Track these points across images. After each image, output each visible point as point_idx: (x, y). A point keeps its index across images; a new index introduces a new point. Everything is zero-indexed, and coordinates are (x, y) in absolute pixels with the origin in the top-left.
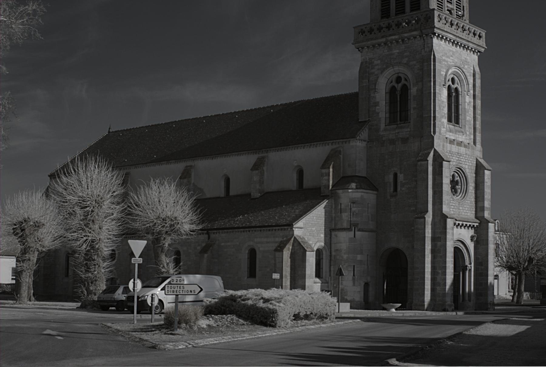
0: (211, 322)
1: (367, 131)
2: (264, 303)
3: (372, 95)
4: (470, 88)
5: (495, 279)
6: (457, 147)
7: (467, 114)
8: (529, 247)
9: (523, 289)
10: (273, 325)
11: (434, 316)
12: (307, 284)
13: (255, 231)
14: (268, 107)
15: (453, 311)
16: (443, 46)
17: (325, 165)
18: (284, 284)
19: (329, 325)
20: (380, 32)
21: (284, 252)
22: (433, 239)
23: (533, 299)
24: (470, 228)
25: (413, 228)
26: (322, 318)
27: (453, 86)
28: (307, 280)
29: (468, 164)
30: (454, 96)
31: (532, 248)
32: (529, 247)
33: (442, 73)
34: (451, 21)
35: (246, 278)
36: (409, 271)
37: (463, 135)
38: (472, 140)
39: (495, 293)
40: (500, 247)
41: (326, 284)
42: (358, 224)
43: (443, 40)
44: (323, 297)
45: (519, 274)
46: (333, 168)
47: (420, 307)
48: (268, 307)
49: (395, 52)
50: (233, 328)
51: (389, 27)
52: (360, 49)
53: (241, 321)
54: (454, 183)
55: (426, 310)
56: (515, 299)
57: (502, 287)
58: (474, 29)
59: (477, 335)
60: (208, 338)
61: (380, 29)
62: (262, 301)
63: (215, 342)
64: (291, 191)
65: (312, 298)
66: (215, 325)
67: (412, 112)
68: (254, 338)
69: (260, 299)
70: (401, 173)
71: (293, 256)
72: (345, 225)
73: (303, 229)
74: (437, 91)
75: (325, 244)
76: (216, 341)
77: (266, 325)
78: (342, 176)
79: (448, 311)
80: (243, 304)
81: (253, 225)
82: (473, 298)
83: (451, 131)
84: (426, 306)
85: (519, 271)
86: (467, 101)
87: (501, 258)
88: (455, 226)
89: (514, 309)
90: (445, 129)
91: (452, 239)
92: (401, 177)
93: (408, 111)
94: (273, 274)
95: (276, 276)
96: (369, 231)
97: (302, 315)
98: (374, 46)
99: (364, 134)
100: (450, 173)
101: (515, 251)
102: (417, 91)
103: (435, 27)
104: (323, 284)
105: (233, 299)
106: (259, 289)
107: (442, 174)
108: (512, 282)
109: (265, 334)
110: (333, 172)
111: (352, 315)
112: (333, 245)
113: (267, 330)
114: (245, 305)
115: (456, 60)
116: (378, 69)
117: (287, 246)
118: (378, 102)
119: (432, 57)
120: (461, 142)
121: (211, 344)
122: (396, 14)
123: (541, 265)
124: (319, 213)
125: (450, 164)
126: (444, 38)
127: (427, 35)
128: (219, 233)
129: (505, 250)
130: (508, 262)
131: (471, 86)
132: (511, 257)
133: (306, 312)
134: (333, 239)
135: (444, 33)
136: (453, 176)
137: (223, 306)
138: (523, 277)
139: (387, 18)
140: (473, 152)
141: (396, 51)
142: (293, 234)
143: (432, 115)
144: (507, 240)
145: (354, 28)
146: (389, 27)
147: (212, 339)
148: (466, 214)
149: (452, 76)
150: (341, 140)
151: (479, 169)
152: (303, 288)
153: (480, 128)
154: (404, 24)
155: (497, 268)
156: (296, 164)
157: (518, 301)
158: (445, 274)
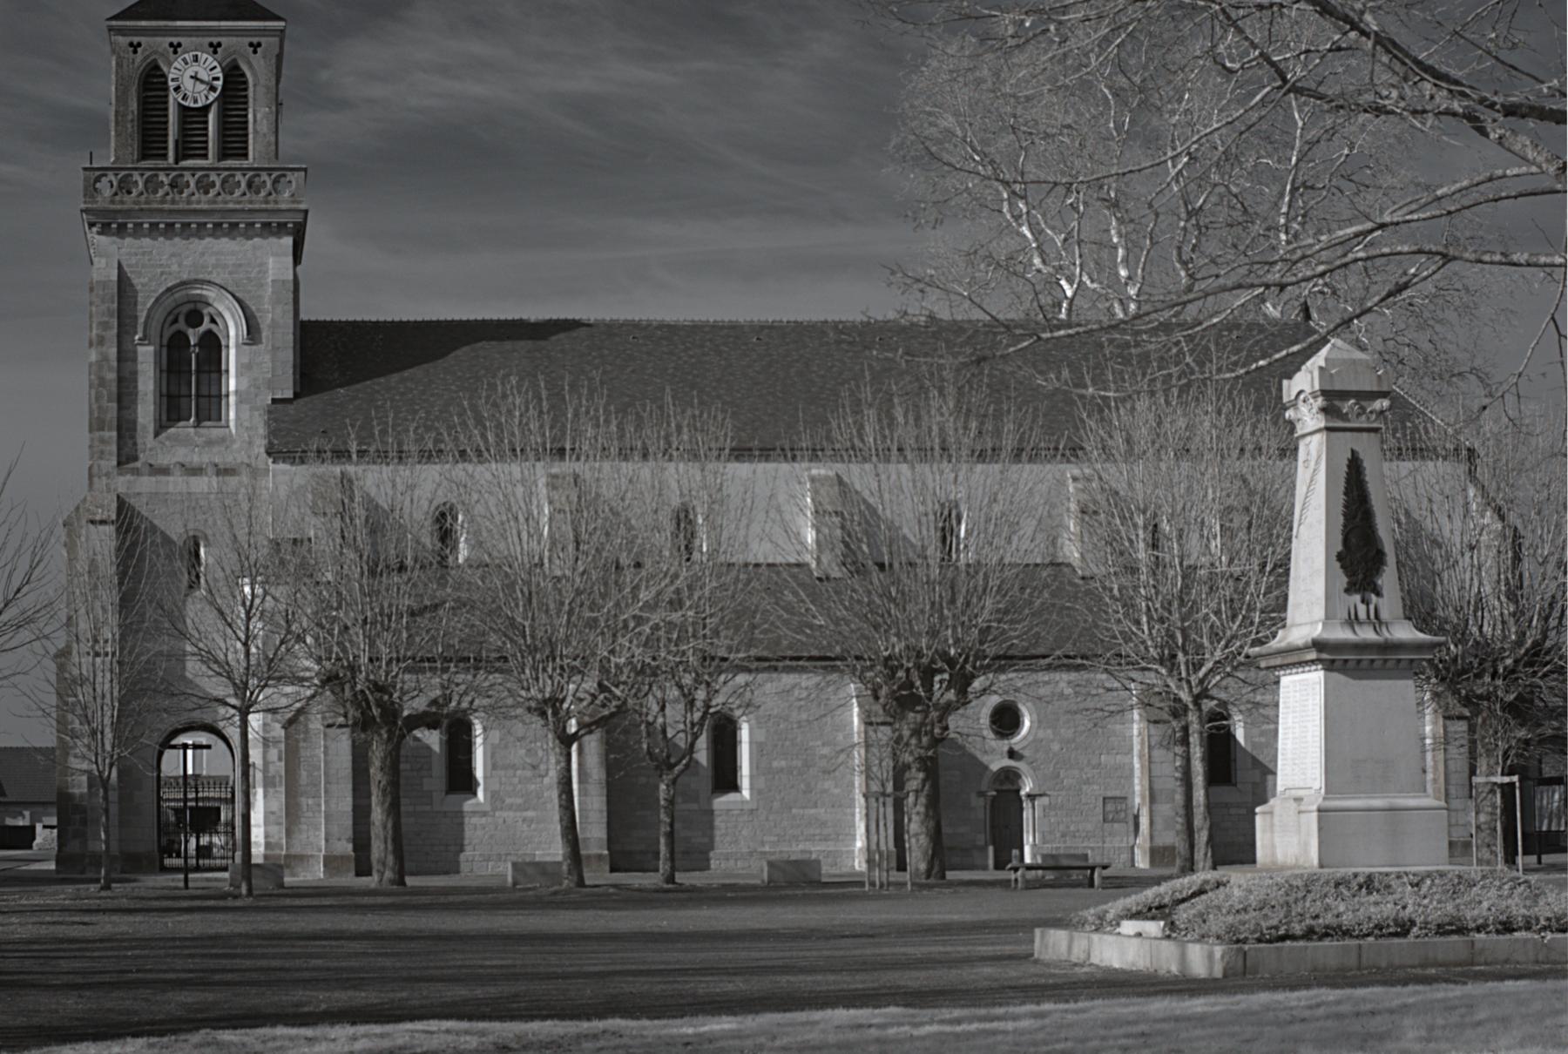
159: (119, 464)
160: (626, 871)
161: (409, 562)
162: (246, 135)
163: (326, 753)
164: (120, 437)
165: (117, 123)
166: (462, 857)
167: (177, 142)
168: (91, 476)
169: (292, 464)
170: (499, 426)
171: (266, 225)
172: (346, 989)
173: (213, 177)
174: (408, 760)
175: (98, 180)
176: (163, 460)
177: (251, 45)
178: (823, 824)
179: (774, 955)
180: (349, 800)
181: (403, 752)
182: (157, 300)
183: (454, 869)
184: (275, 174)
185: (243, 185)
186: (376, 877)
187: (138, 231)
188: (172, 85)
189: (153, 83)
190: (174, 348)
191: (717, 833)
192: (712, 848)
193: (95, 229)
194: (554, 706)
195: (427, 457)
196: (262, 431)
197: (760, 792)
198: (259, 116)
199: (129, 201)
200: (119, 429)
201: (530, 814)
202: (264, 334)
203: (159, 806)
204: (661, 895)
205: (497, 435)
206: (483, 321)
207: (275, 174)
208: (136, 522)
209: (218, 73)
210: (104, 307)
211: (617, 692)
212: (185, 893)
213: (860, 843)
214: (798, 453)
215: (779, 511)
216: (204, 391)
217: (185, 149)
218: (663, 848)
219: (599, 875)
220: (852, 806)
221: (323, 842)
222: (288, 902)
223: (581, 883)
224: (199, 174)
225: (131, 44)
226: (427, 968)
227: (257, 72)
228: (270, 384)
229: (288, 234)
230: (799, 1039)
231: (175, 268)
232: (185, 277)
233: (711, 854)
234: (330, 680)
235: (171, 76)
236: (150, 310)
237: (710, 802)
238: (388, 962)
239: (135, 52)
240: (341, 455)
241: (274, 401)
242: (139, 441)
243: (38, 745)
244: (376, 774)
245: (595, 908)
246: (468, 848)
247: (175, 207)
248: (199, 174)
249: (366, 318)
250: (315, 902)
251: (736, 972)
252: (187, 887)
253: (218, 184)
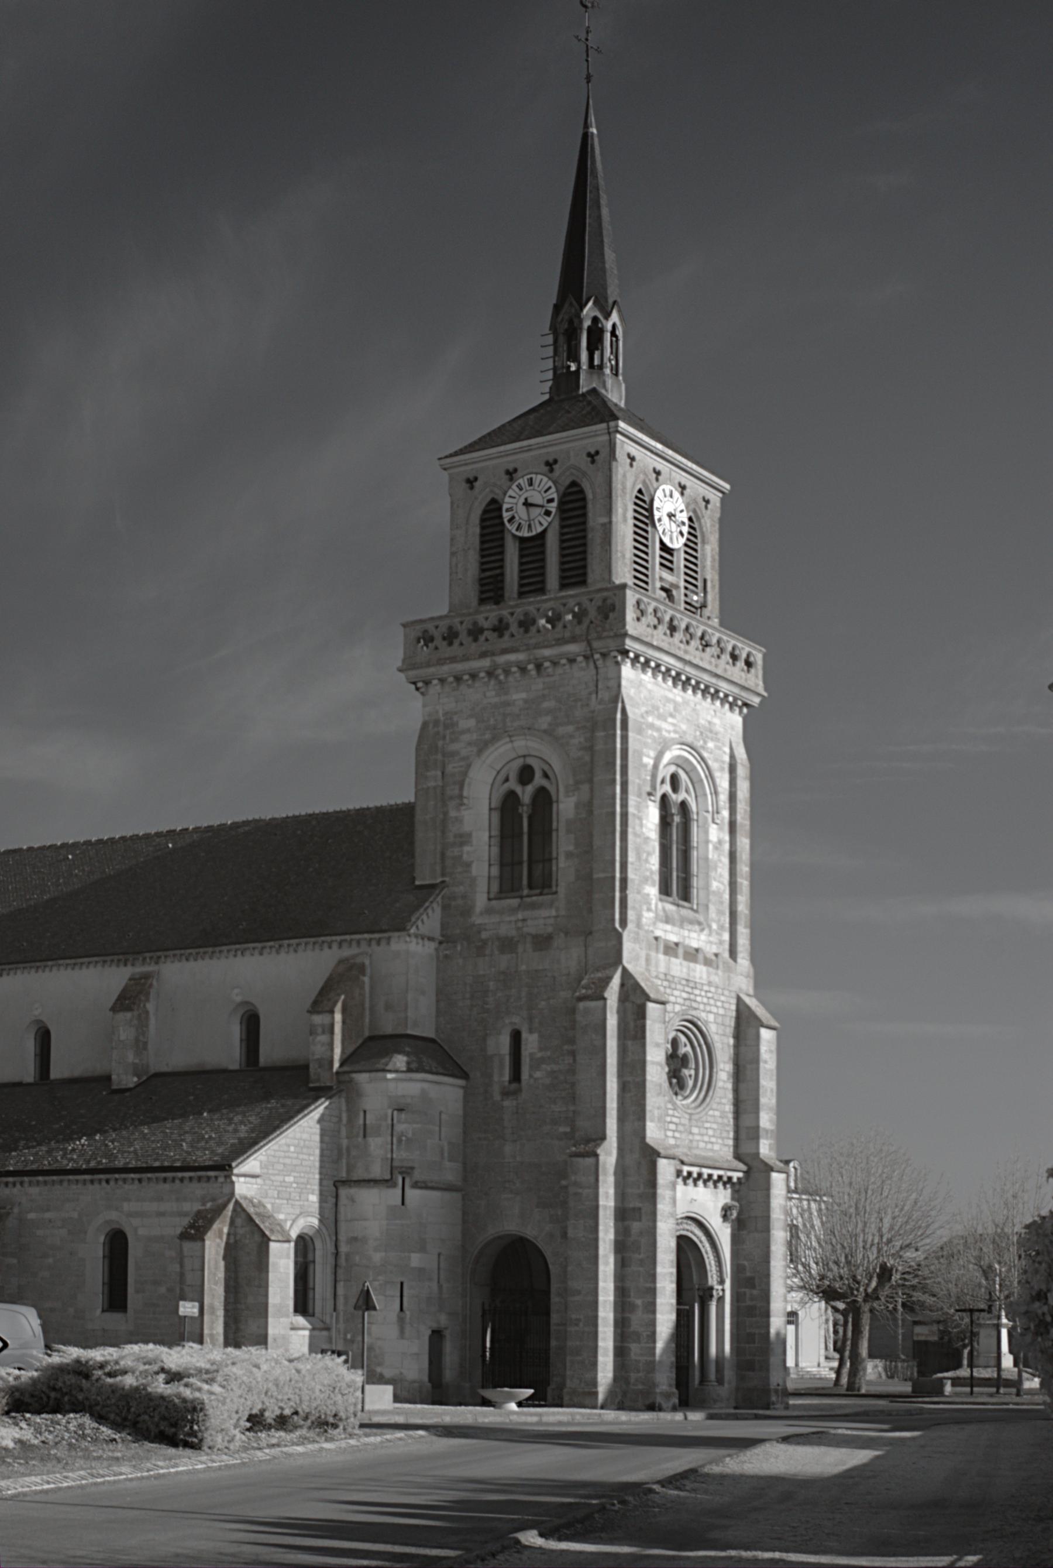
0: (26, 1433)
1: (438, 910)
2: (167, 1383)
3: (453, 814)
4: (721, 803)
5: (789, 1322)
6: (685, 963)
7: (713, 874)
8: (881, 1236)
9: (864, 1351)
10: (192, 1443)
11: (623, 1423)
12: (271, 1331)
13: (125, 1180)
14: (158, 835)
15: (674, 1409)
16: (650, 686)
17: (321, 1003)
18: (206, 1331)
19: (343, 1444)
20: (476, 640)
21: (207, 1243)
22: (622, 1215)
23: (891, 1377)
24: (720, 1185)
25: (564, 1183)
26: (325, 1424)
27: (674, 796)
28: (270, 1320)
29: (714, 1010)
30: (677, 824)
31: (889, 1241)
32: (881, 1236)
33: (645, 760)
34: (671, 620)
35: (99, 1311)
36: (555, 1299)
37: (702, 930)
38: (727, 946)
39: (790, 1363)
40: (802, 1237)
41: (325, 1333)
42: (412, 1168)
43: (650, 672)
44: (326, 1368)
45: (853, 1311)
46: (344, 1011)
47: (586, 1397)
48: (178, 1396)
49: (515, 697)
50: (86, 1449)
51: (500, 628)
52: (421, 685)
53: (106, 1431)
54: (676, 1062)
55: (602, 1408)
56: (844, 1380)
57: (807, 1345)
58: (733, 642)
59: (742, 1476)
60: (24, 1475)
61: (476, 632)
62: (162, 1377)
63: (46, 1487)
64: (225, 1071)
65: (298, 1371)
66: (36, 1442)
67: (562, 865)
68: (149, 1478)
69: (157, 1373)
70: (531, 1031)
71: (231, 1253)
72: (377, 1170)
73: (259, 1180)
74: (631, 810)
75: (320, 1221)
76: (48, 1483)
77: (173, 1442)
78: (367, 1034)
79: (660, 1409)
80: (111, 1385)
81: (119, 1163)
82: (729, 1374)
83: (667, 920)
84: (601, 1397)
85: (855, 1301)
86: (712, 838)
87: (804, 1265)
88: (680, 1180)
89: (840, 1406)
90: (651, 915)
91: (673, 1215)
92: (531, 1042)
93: (550, 860)
94: (181, 1303)
95: (188, 1308)
96: (445, 1189)
97: (269, 1416)
98: (458, 679)
99: (430, 920)
100: (667, 1034)
101: (843, 1247)
102: (577, 806)
103: (626, 635)
104: (316, 1333)
105: (81, 1370)
106: (151, 1346)
107: (644, 1037)
108: (836, 1332)
109: (176, 1466)
110: (344, 1022)
111: (400, 1420)
112: (343, 1227)
113: (180, 1457)
114: (114, 1389)
115: (684, 727)
116: (470, 744)
117: (215, 1226)
118: (470, 835)
119: (619, 716)
120: (697, 950)
121: (36, 1493)
122: (521, 594)
123: (914, 1288)
124: (305, 1136)
125: (665, 1011)
126: (653, 664)
127: (604, 655)
128: (22, 1183)
129: (815, 1244)
130: (822, 1277)
131: (724, 797)
132: (831, 1265)
133: (282, 1408)
134: (342, 1209)
135: (651, 653)
136: (675, 1042)
137: (54, 1389)
138: (866, 1319)
139: (497, 603)
140: (729, 978)
141: (518, 697)
142: (232, 1194)
143: (618, 875)
144: (820, 1216)
145: (404, 626)
146: (500, 628)
147: (38, 1479)
148: (709, 1146)
149: (673, 769)
150: (366, 936)
151: (745, 1024)
152: (262, 1340)
153: (747, 912)
154: (543, 622)
155: (794, 1294)
156: (239, 999)
157: (851, 1386)
158: (651, 1308)
188: (506, 516)
209: (553, 494)
235: (505, 507)
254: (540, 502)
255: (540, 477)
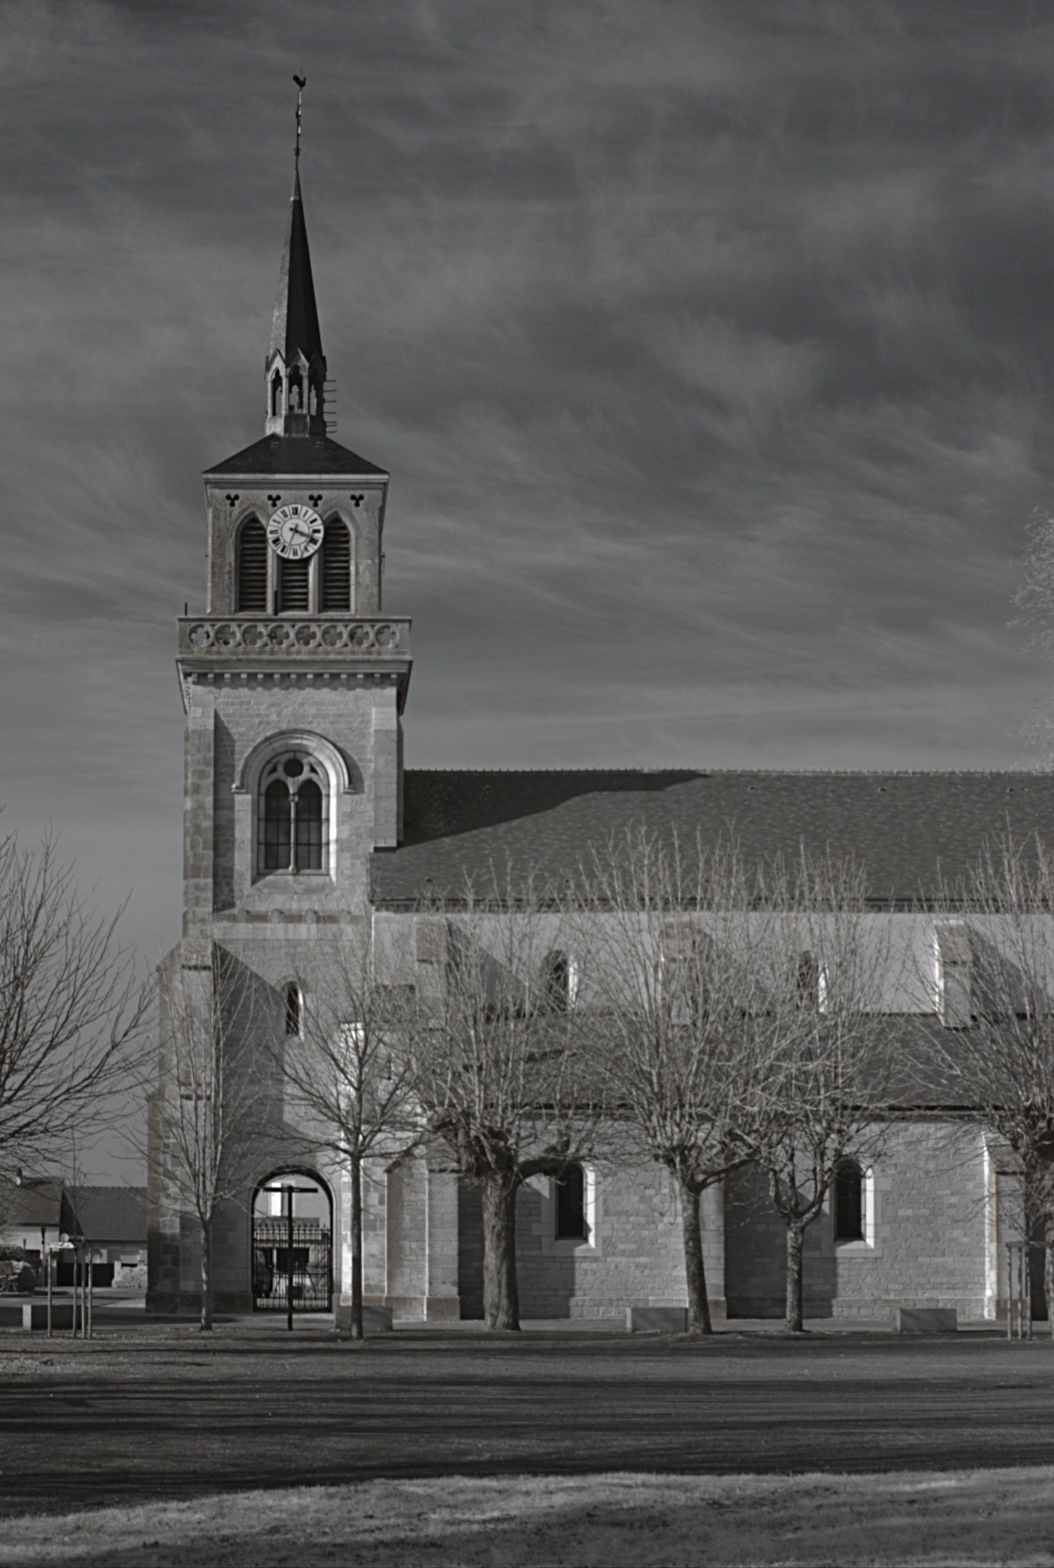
159: (216, 910)
160: (744, 1317)
161: (527, 1007)
162: (348, 587)
163: (430, 1199)
164: (216, 883)
165: (213, 574)
166: (573, 1302)
167: (276, 594)
168: (185, 922)
169: (396, 912)
170: (625, 872)
171: (369, 676)
172: (503, 1437)
173: (314, 628)
174: (517, 1206)
175: (194, 630)
176: (261, 907)
177: (353, 497)
178: (952, 1273)
179: (940, 1406)
180: (455, 1244)
181: (517, 1198)
182: (255, 749)
183: (564, 1313)
184: (378, 626)
185: (345, 636)
186: (489, 1320)
187: (235, 681)
188: (270, 537)
189: (251, 536)
190: (272, 798)
191: (840, 1280)
192: (835, 1296)
193: (190, 679)
194: (682, 1154)
195: (549, 905)
196: (365, 879)
197: (885, 1240)
198: (361, 568)
199: (226, 652)
200: (215, 876)
201: (643, 1260)
202: (367, 783)
203: (253, 1248)
204: (792, 1343)
205: (625, 885)
206: (595, 772)
207: (378, 626)
208: (240, 969)
209: (319, 525)
210: (199, 756)
211: (750, 1140)
212: (289, 1334)
213: (989, 1292)
214: (936, 904)
215: (915, 962)
216: (303, 839)
217: (284, 600)
218: (790, 1296)
219: (720, 1322)
220: (982, 1255)
221: (427, 1286)
222: (401, 1345)
223: (708, 1330)
224: (299, 625)
225: (228, 497)
226: (577, 1416)
227: (358, 526)
228: (373, 834)
229: (392, 685)
230: (1032, 1498)
231: (274, 717)
232: (284, 726)
233: (834, 1302)
234: (443, 1126)
235: (269, 529)
236: (247, 760)
237: (832, 1250)
238: (534, 1409)
239: (232, 505)
240: (455, 903)
241: (377, 849)
242: (236, 888)
243: (135, 1185)
244: (490, 1219)
245: (727, 1355)
246: (578, 1293)
247: (275, 657)
248: (299, 625)
249: (472, 768)
250: (430, 1345)
251: (910, 1424)
252: (290, 1328)
253: (319, 635)
254: (306, 530)
255: (305, 508)
